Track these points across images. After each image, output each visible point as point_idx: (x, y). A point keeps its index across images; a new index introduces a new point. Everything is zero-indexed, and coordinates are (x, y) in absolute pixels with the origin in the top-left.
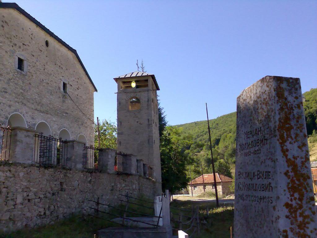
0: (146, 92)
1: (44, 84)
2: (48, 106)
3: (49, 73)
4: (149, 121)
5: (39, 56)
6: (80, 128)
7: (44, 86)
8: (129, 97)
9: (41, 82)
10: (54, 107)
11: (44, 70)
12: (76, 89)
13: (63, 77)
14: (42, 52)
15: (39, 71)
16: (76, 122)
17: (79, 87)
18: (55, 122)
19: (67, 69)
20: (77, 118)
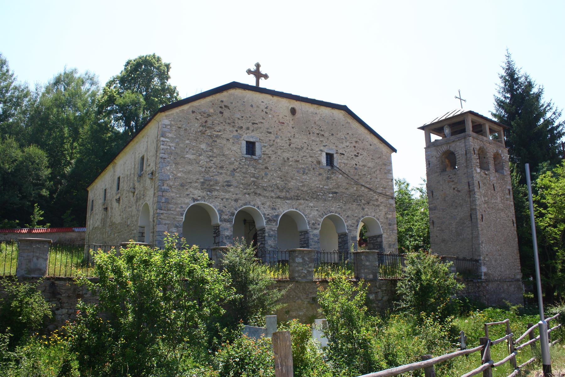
0: (463, 141)
4: (469, 186)
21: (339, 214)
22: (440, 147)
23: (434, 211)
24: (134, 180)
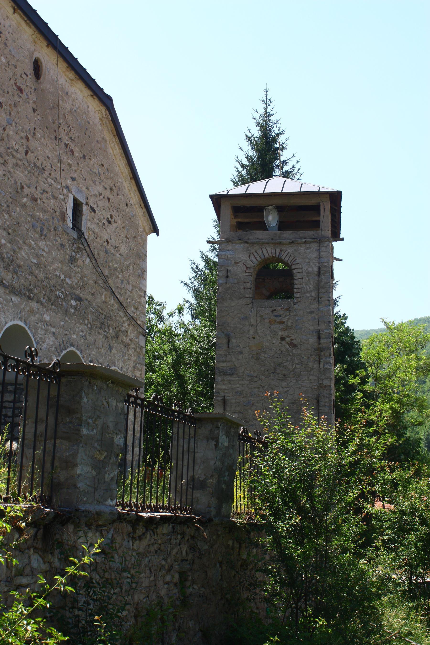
0: (315, 246)
1: (25, 200)
2: (31, 273)
3: (39, 164)
4: (319, 338)
5: (15, 106)
6: (111, 349)
7: (24, 206)
8: (258, 258)
9: (17, 192)
10: (48, 278)
11: (26, 153)
12: (105, 221)
13: (73, 179)
14: (24, 96)
15: (14, 157)
16: (101, 328)
17: (111, 216)
18: (49, 327)
19: (84, 157)
20: (106, 317)
21: (81, 352)
22: (257, 247)
23: (229, 378)
24: (116, 160)
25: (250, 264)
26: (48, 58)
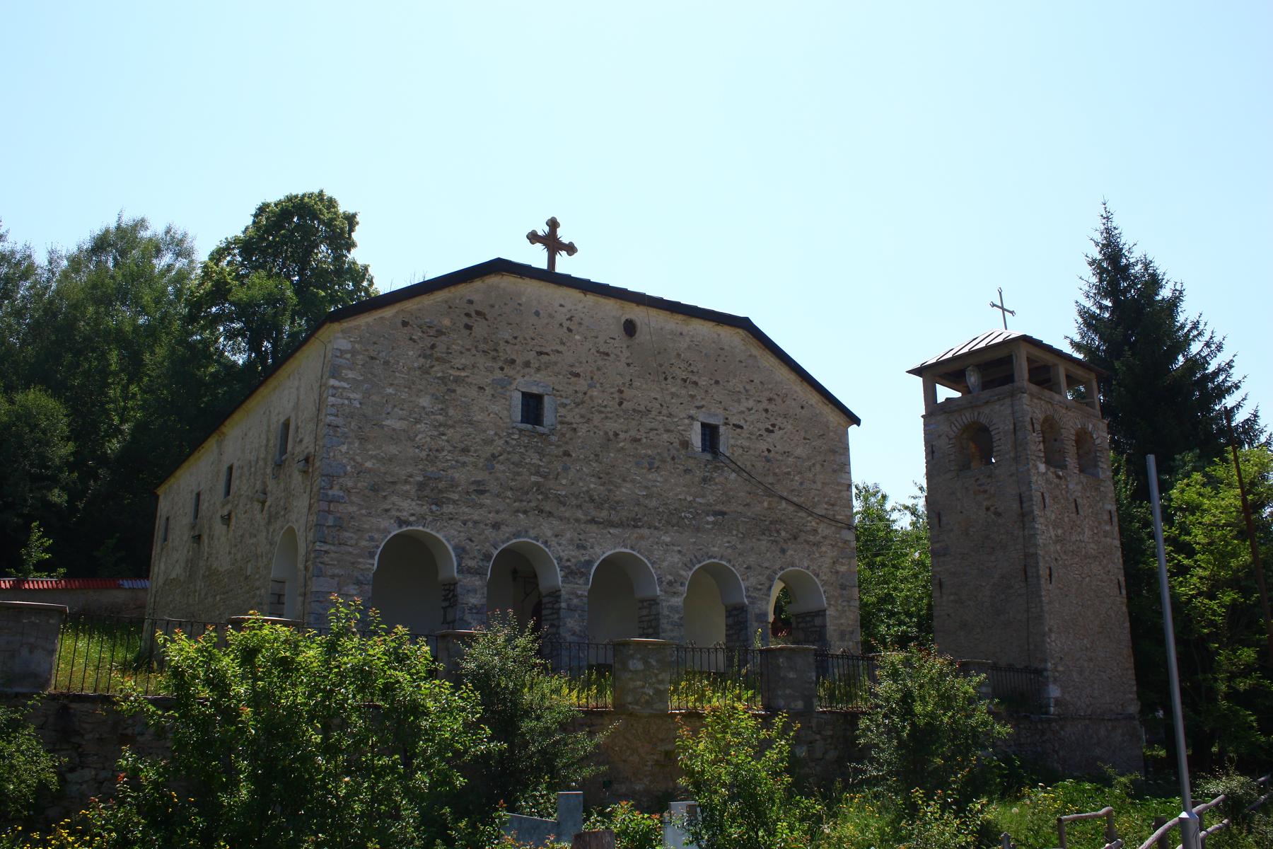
0: (1008, 401)
4: (1021, 502)
25: (952, 434)
26: (637, 313)
